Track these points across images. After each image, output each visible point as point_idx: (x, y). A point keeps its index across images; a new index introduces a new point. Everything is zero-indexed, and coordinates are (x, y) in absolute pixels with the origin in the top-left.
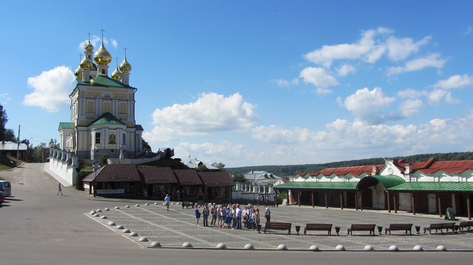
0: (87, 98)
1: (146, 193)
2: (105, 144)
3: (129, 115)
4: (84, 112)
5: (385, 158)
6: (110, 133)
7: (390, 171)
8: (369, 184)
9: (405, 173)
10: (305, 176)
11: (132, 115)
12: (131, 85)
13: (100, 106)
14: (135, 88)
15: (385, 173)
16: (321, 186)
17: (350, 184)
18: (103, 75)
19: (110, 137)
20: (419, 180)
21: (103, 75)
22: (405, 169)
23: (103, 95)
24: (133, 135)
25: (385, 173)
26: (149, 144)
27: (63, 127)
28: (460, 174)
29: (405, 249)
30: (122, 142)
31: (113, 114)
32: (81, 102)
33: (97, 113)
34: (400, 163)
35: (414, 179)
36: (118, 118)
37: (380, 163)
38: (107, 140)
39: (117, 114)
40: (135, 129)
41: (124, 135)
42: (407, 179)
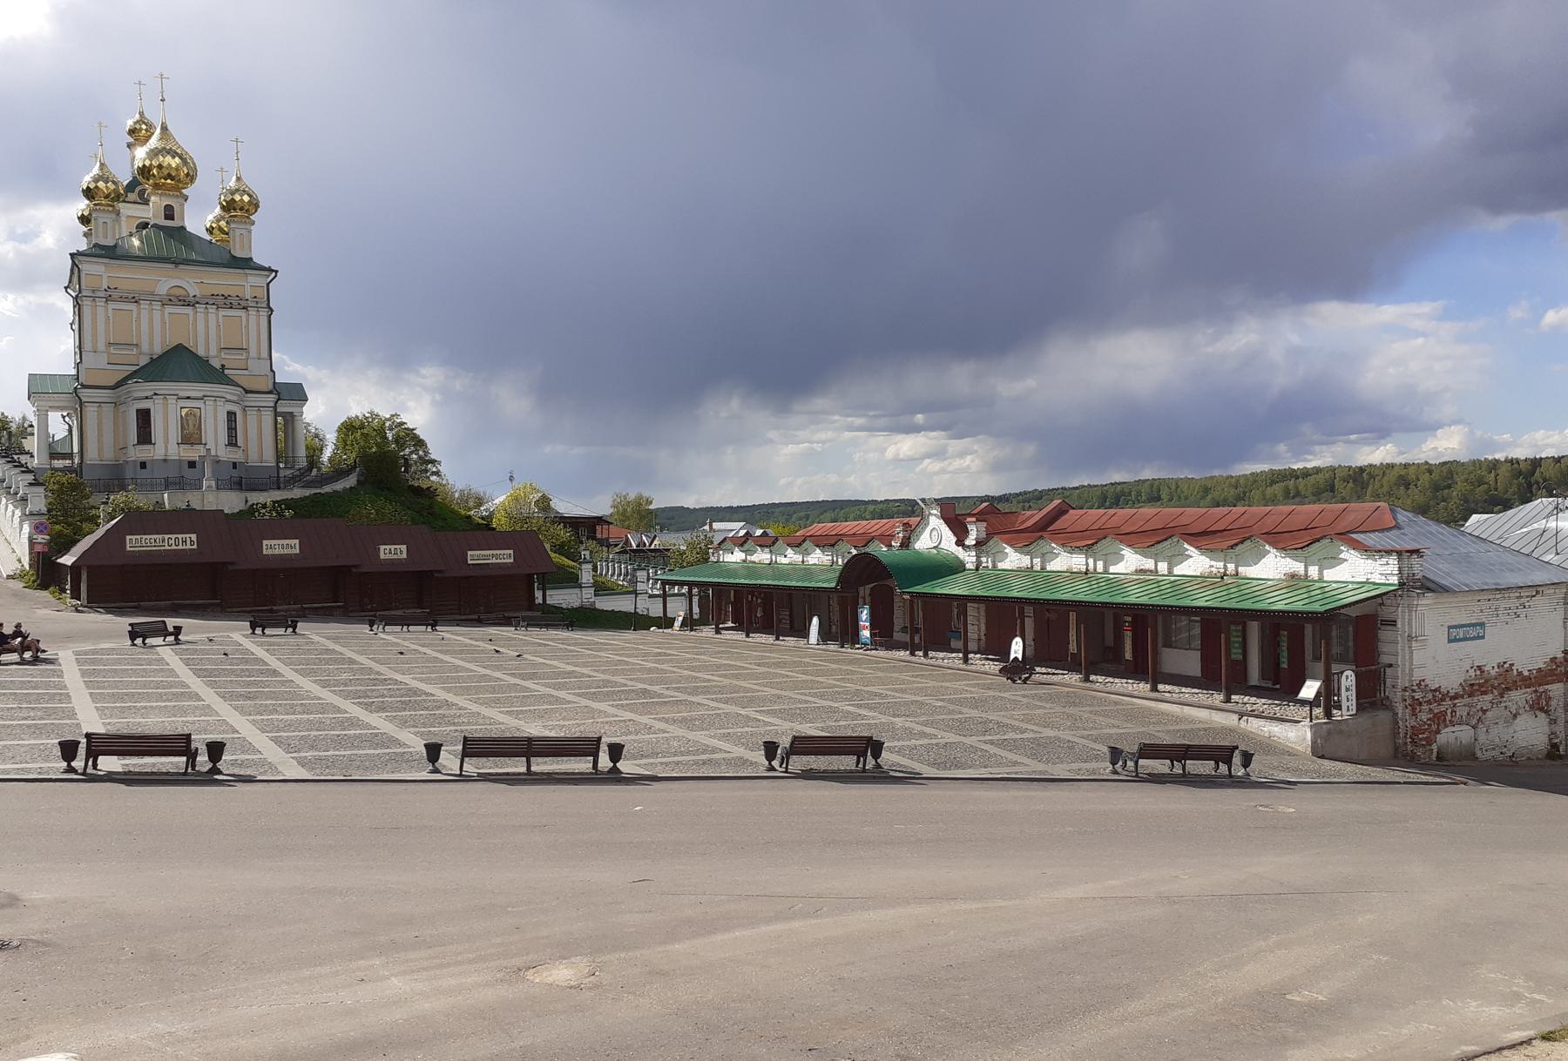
0: (108, 299)
1: (1191, 663)
2: (166, 442)
3: (253, 353)
4: (101, 346)
5: (923, 500)
6: (184, 412)
7: (935, 538)
8: (865, 574)
9: (967, 542)
10: (746, 546)
11: (265, 354)
12: (258, 259)
13: (155, 331)
14: (270, 270)
15: (923, 543)
16: (1254, 597)
17: (808, 571)
18: (169, 223)
19: (184, 422)
20: (1177, 570)
21: (169, 223)
22: (966, 532)
23: (162, 289)
24: (268, 418)
25: (923, 543)
26: (421, 434)
27: (39, 388)
28: (1088, 549)
29: (1060, 771)
30: (223, 437)
31: (201, 352)
32: (87, 311)
33: (145, 347)
34: (955, 514)
35: (986, 561)
36: (216, 364)
37: (909, 512)
38: (174, 434)
39: (213, 352)
40: (273, 397)
41: (231, 415)
42: (969, 558)
